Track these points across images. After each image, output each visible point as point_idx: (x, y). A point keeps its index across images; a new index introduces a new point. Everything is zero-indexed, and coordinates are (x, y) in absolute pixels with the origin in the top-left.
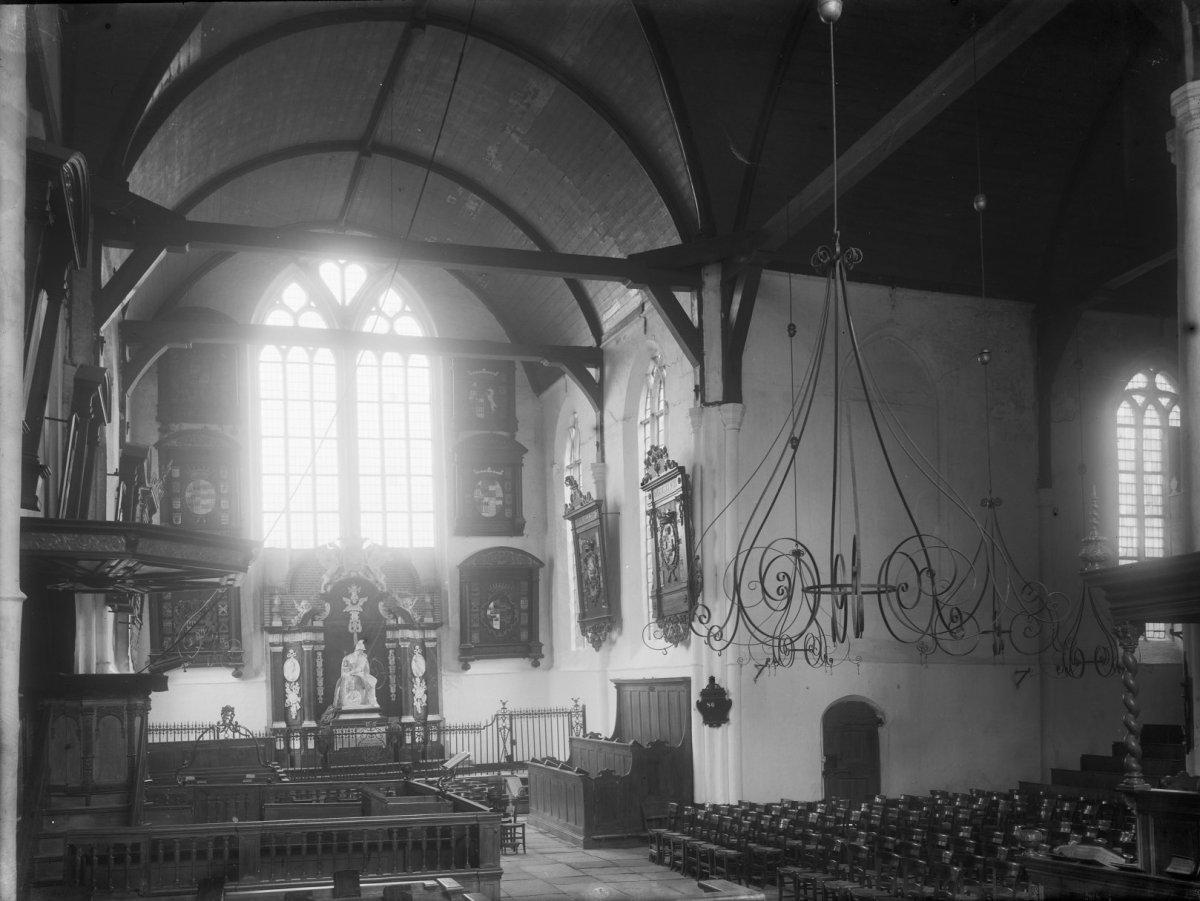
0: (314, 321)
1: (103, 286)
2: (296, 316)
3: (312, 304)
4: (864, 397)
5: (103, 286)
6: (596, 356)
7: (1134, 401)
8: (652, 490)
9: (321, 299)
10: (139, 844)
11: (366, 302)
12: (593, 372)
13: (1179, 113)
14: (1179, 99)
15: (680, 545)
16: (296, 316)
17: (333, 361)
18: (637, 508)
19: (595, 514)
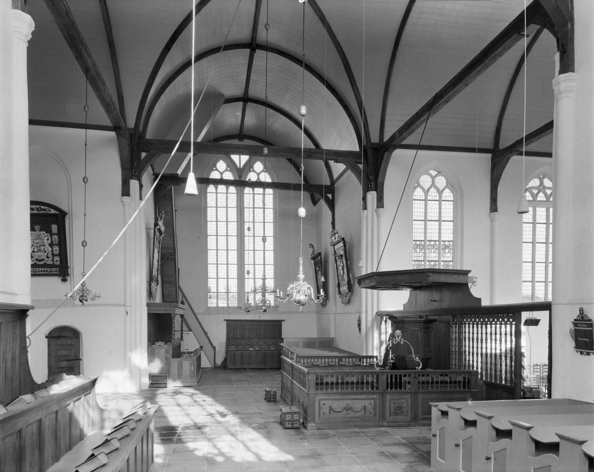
0: (228, 176)
1: (142, 158)
2: (222, 174)
3: (228, 169)
4: (199, 317)
5: (142, 158)
6: (331, 189)
7: (546, 193)
8: (334, 246)
9: (231, 165)
10: (172, 357)
11: (249, 166)
12: (330, 196)
13: (555, 88)
14: (556, 82)
15: (237, 140)
16: (222, 174)
17: (235, 192)
18: (245, 298)
19: (341, 244)
